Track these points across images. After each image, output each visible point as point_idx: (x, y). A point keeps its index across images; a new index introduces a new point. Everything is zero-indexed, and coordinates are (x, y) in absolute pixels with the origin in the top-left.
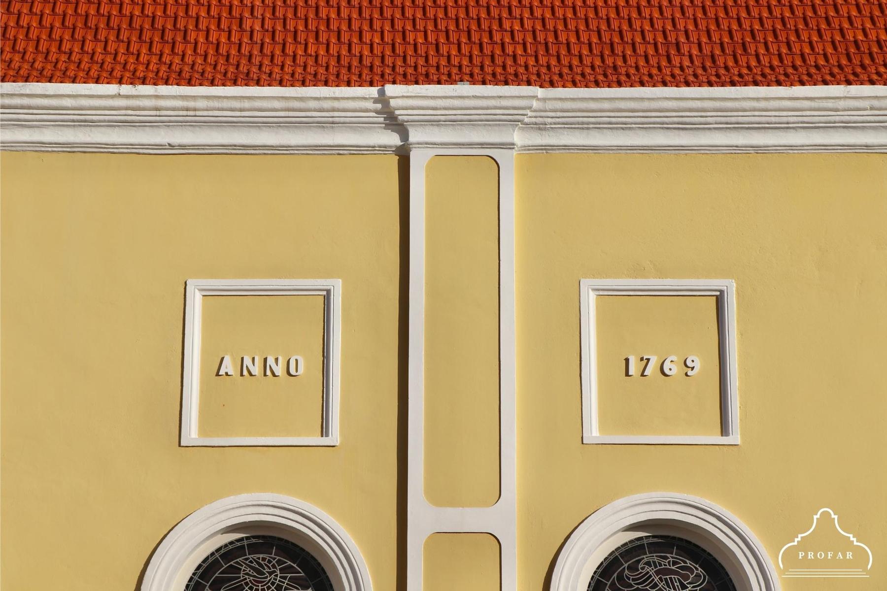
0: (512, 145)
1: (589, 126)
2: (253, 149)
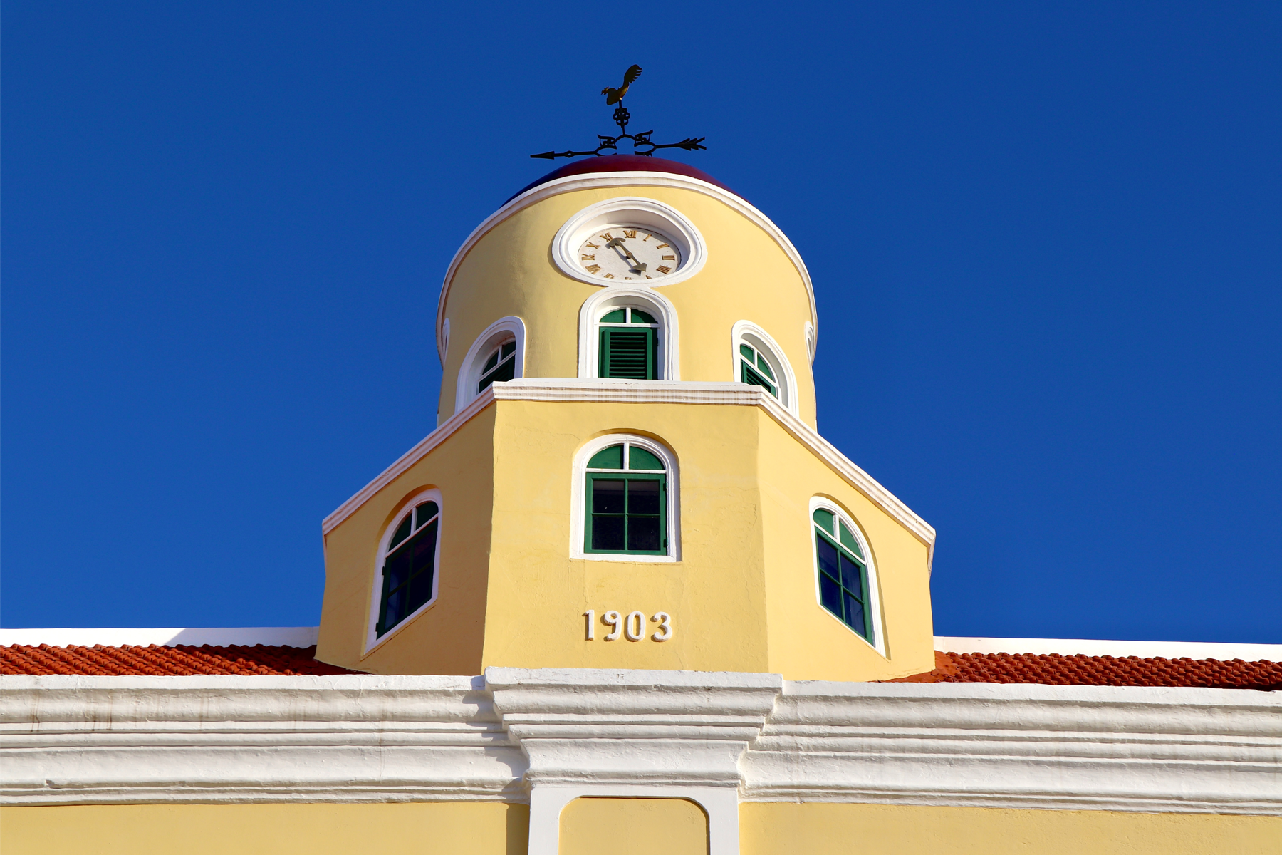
0: (733, 779)
1: (883, 755)
2: (220, 792)
